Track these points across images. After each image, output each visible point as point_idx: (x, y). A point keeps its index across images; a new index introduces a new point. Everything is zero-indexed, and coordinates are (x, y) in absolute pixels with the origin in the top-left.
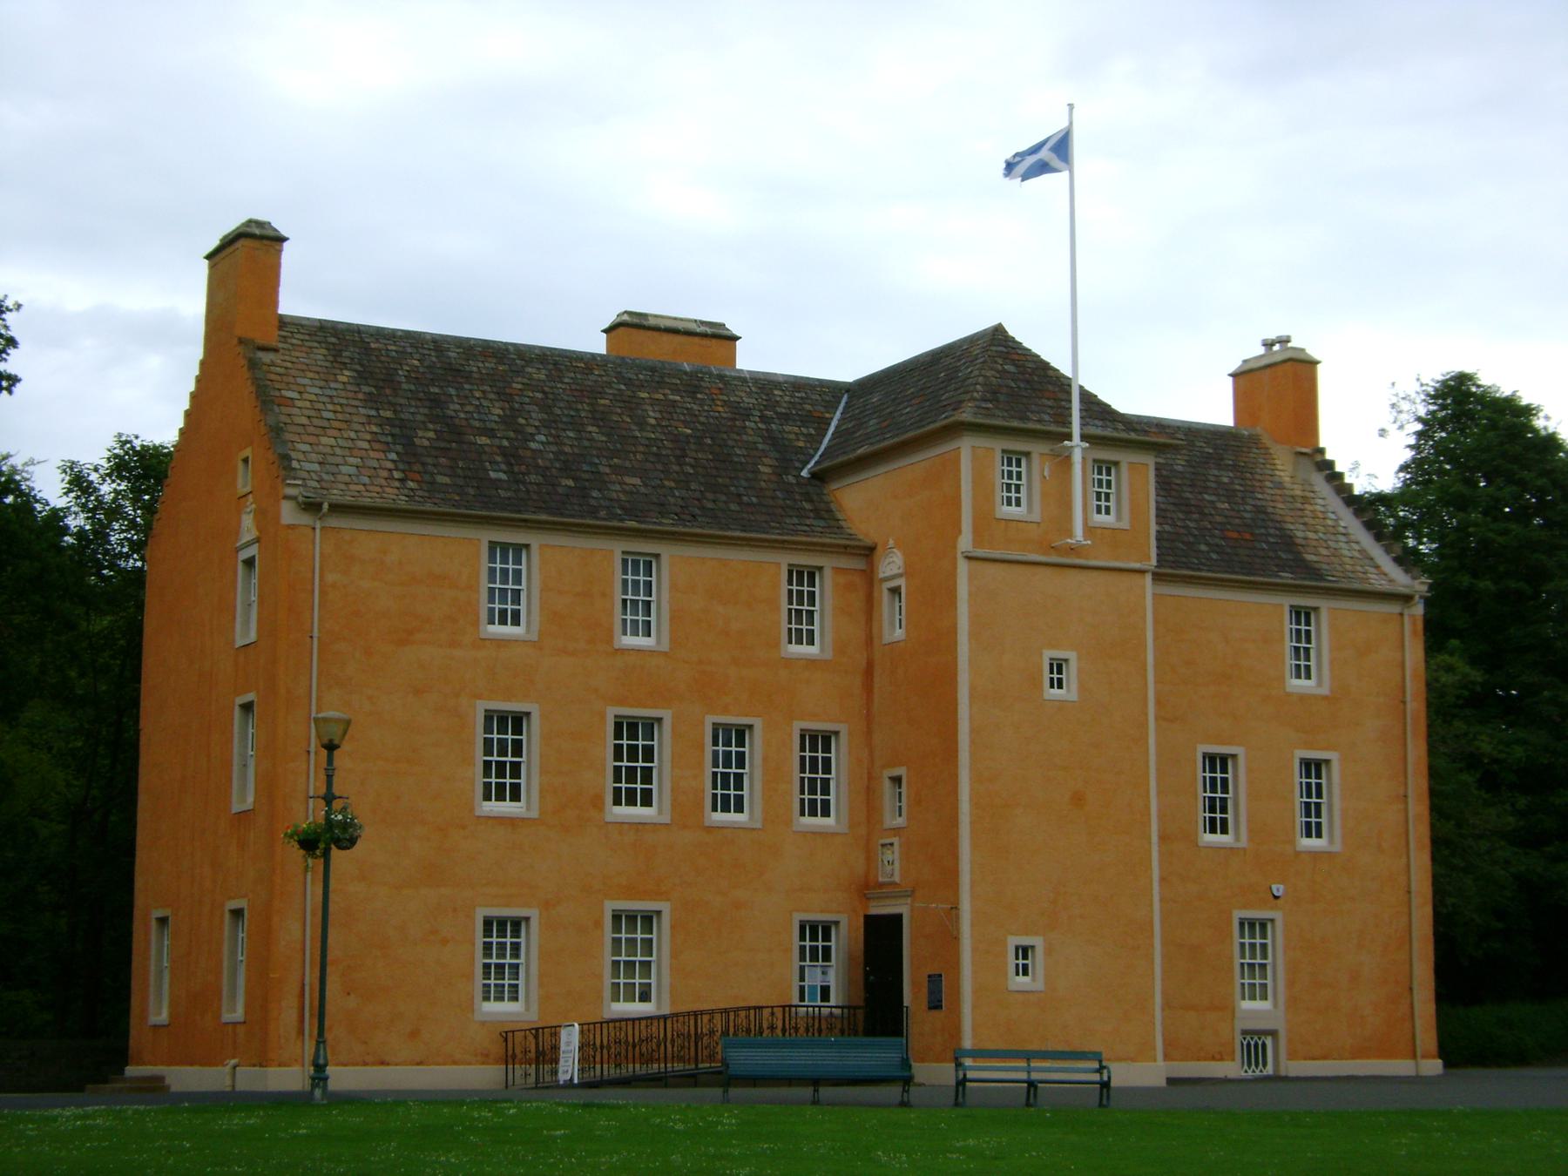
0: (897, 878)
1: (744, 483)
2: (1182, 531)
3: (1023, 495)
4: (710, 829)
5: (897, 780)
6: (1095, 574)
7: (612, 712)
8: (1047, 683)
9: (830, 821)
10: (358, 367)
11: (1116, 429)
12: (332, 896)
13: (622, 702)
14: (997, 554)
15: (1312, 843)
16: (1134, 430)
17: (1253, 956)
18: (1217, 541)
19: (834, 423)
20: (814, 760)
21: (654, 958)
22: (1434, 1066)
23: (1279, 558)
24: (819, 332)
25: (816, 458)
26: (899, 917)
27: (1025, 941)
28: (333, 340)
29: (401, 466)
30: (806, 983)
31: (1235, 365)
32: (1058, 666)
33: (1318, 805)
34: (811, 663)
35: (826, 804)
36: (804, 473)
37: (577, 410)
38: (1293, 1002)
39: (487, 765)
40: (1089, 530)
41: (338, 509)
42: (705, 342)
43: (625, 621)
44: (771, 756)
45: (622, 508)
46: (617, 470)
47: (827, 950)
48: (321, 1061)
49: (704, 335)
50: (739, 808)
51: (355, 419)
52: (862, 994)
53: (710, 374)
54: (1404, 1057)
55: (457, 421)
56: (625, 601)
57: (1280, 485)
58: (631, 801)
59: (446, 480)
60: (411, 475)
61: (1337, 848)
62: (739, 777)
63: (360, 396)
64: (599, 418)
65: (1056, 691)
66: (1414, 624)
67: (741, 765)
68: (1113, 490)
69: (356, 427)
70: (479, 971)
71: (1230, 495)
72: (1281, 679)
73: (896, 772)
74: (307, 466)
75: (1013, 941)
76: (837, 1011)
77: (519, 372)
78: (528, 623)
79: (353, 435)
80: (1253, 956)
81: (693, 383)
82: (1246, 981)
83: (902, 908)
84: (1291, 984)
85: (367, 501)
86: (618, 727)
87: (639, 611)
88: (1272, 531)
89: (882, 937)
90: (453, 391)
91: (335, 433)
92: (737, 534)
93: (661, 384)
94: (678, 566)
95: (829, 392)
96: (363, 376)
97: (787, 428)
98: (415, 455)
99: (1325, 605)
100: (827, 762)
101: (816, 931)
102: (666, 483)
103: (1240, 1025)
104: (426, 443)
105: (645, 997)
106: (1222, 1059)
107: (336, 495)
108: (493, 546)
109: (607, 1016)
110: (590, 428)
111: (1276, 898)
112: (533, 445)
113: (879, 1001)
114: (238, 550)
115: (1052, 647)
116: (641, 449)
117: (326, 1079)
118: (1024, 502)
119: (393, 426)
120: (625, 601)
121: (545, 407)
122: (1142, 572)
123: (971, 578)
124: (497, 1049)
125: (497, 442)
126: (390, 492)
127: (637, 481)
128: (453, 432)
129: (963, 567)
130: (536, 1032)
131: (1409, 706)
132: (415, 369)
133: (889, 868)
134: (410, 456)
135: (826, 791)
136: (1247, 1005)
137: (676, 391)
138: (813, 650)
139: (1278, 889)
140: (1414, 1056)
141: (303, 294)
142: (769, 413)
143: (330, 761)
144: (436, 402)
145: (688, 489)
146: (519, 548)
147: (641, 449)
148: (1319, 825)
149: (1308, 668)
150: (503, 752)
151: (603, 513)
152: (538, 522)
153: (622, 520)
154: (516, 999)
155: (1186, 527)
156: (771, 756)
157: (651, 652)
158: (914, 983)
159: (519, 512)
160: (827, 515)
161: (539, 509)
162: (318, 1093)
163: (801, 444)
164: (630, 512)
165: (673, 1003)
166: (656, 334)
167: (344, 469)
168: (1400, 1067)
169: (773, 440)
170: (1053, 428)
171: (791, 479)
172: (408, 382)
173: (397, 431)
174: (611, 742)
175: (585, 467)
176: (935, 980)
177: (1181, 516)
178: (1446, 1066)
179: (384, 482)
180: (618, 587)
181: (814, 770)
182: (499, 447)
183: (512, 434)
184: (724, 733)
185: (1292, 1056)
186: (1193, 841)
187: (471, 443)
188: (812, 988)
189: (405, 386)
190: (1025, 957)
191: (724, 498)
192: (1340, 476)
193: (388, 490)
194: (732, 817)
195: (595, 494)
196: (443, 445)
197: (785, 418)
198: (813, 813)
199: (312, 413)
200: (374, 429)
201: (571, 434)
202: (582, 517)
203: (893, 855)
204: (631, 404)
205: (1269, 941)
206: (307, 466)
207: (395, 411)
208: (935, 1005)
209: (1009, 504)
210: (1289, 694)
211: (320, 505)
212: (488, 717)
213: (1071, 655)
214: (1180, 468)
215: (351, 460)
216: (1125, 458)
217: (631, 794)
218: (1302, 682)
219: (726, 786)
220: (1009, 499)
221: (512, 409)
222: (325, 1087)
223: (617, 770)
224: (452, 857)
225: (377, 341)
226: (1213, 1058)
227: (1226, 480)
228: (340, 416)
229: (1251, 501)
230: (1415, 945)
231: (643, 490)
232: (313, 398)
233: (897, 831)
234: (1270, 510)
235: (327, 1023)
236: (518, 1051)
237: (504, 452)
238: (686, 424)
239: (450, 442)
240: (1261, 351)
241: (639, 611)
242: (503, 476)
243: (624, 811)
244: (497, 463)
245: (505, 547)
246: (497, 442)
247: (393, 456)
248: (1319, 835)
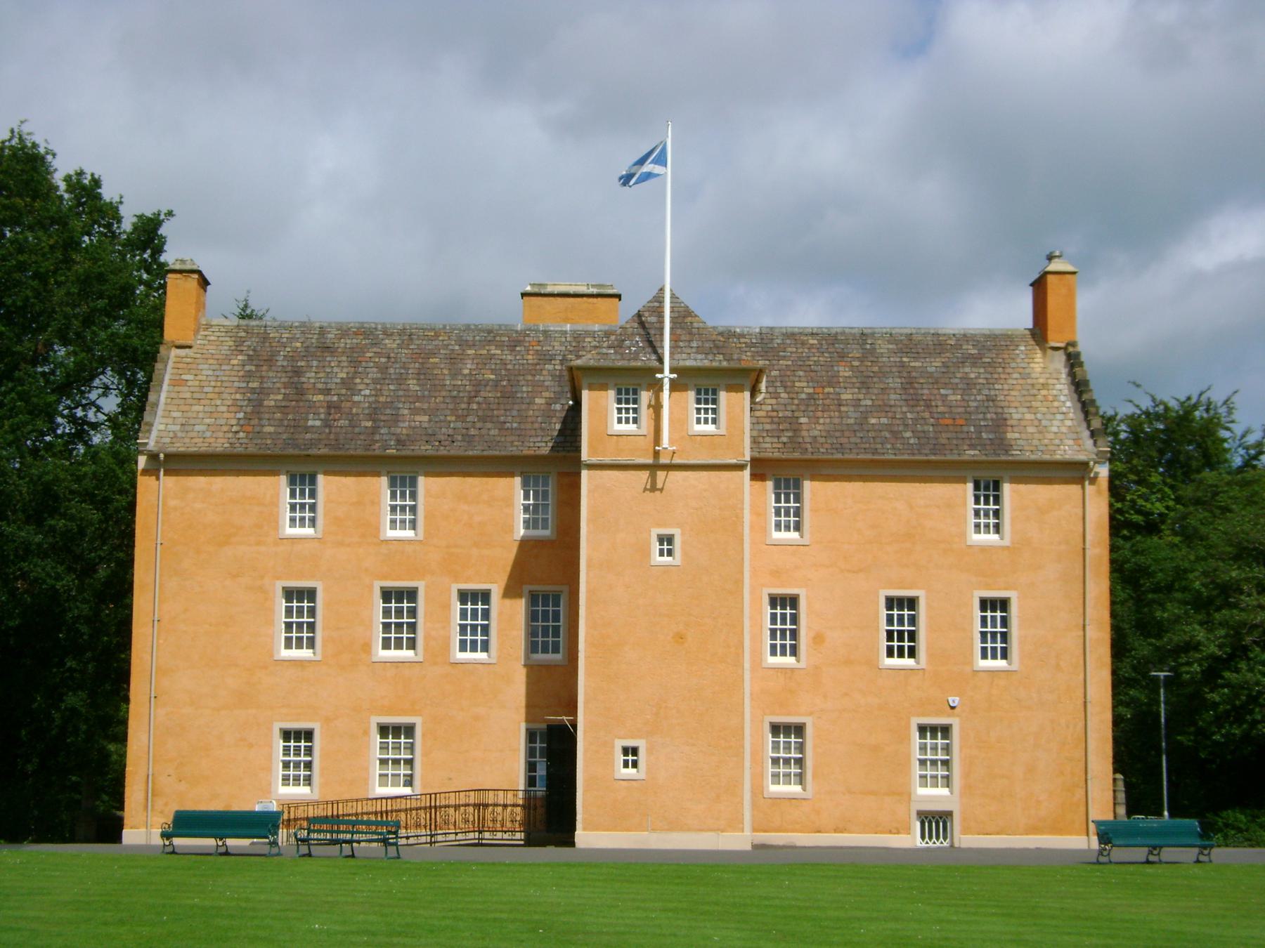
13: (385, 578)
27: (630, 743)
38: (968, 789)
53: (537, 331)
54: (1078, 834)
72: (963, 535)
84: (966, 775)
103: (915, 808)
111: (953, 708)
115: (659, 526)
122: (740, 467)
136: (922, 791)
137: (500, 346)
139: (954, 700)
150: (545, 619)
157: (410, 541)
165: (424, 786)
185: (966, 831)
186: (873, 664)
226: (890, 832)
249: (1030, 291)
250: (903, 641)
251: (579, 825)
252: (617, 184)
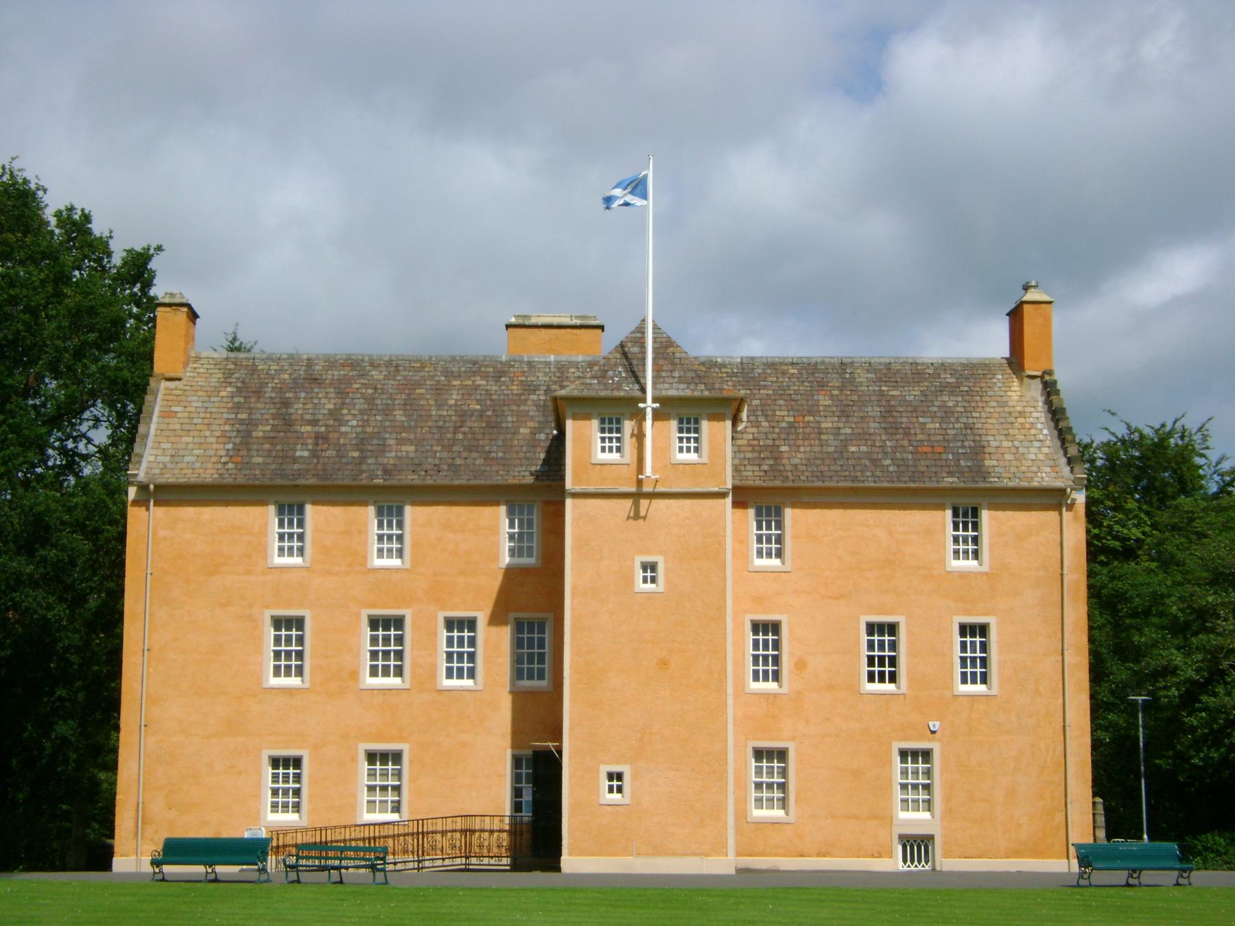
4: (442, 691)
13: (373, 606)
27: (615, 768)
38: (949, 813)
53: (521, 362)
61: (994, 692)
72: (943, 561)
84: (947, 799)
91: (197, 433)
103: (897, 831)
106: (881, 857)
111: (933, 732)
115: (642, 553)
122: (722, 495)
123: (574, 507)
136: (903, 815)
139: (935, 725)
157: (397, 570)
165: (411, 813)
166: (536, 330)
185: (947, 854)
186: (854, 689)
213: (659, 559)
226: (873, 856)
250: (884, 667)
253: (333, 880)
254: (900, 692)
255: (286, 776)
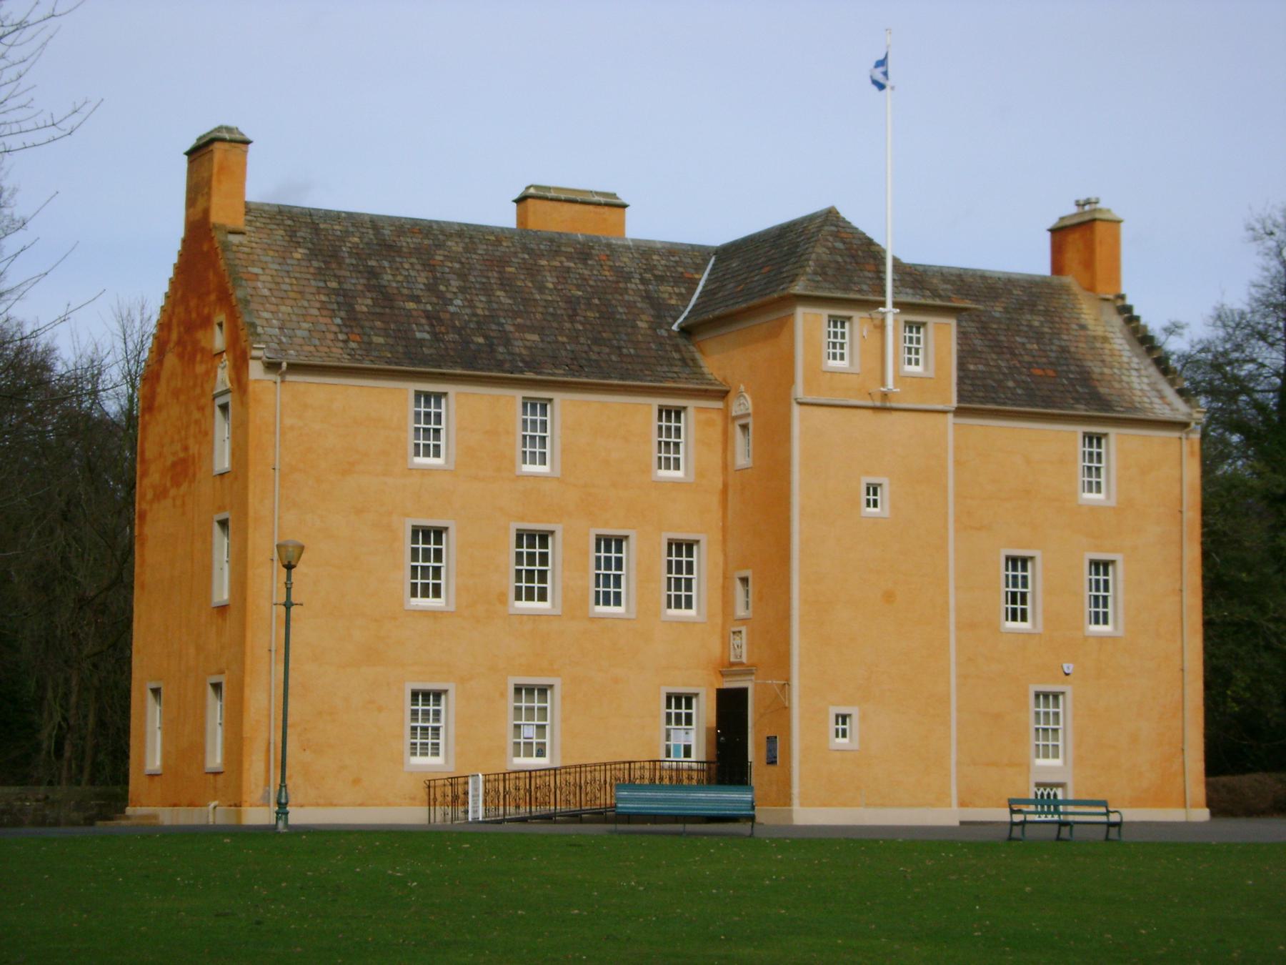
0: (744, 660)
1: (625, 338)
2: (994, 370)
3: (846, 351)
5: (745, 581)
6: (901, 414)
7: (514, 526)
8: (864, 503)
9: (692, 613)
10: (310, 245)
11: (924, 296)
12: (291, 673)
13: (522, 519)
14: (822, 400)
15: (1101, 628)
16: (940, 297)
17: (1047, 722)
18: (1024, 378)
19: (702, 283)
20: (679, 564)
21: (548, 722)
22: (1203, 814)
23: (1077, 392)
24: (690, 202)
25: (686, 313)
26: (743, 693)
28: (289, 222)
29: (345, 330)
30: (672, 743)
31: (1052, 221)
32: (873, 489)
33: (1105, 598)
34: (675, 484)
35: (689, 599)
36: (675, 327)
37: (488, 278)
39: (414, 569)
40: (899, 378)
41: (295, 368)
42: (600, 209)
43: (525, 453)
44: (644, 562)
45: (523, 361)
46: (520, 328)
47: (689, 717)
48: (283, 801)
49: (598, 204)
50: (618, 602)
51: (307, 290)
52: (714, 751)
55: (390, 291)
56: (524, 437)
57: (1083, 327)
58: (530, 597)
59: (381, 340)
60: (352, 337)
62: (618, 578)
63: (312, 270)
64: (506, 283)
65: (871, 509)
66: (1192, 446)
67: (619, 567)
68: (921, 345)
69: (309, 297)
70: (408, 731)
71: (1039, 337)
73: (744, 573)
74: (269, 330)
75: (834, 710)
76: (694, 765)
77: (439, 246)
78: (447, 454)
79: (306, 304)
80: (1047, 722)
81: (584, 252)
82: (1041, 743)
83: (748, 683)
85: (317, 362)
86: (519, 537)
87: (535, 445)
88: (1072, 368)
89: (732, 706)
90: (386, 264)
91: (292, 302)
92: (616, 382)
93: (557, 253)
94: (567, 408)
95: (699, 254)
96: (314, 253)
97: (662, 288)
98: (355, 319)
99: (1113, 432)
100: (690, 564)
101: (680, 700)
102: (560, 339)
104: (365, 309)
105: (541, 753)
107: (293, 356)
108: (418, 394)
109: (510, 768)
110: (498, 293)
111: (1067, 674)
112: (452, 309)
113: (728, 761)
114: (215, 397)
115: (867, 473)
116: (540, 310)
117: (287, 813)
118: (846, 356)
119: (338, 295)
120: (524, 437)
121: (462, 276)
122: (945, 412)
124: (422, 794)
125: (422, 307)
126: (337, 351)
127: (536, 337)
128: (385, 298)
129: (796, 410)
130: (452, 781)
131: (1185, 515)
132: (356, 246)
133: (738, 651)
134: (352, 320)
135: (689, 588)
136: (1041, 762)
137: (570, 258)
138: (680, 474)
139: (1068, 667)
140: (1185, 806)
141: (266, 180)
142: (648, 276)
143: (289, 577)
144: (373, 274)
145: (578, 343)
146: (439, 396)
147: (540, 310)
148: (1105, 614)
149: (1098, 484)
150: (426, 559)
151: (507, 365)
152: (455, 375)
153: (522, 372)
154: (437, 754)
155: (999, 367)
156: (644, 562)
158: (757, 745)
159: (440, 367)
160: (690, 364)
161: (455, 364)
162: (281, 824)
163: (673, 302)
164: (531, 365)
167: (299, 333)
168: (1174, 815)
169: (648, 297)
170: (871, 298)
171: (664, 333)
172: (350, 257)
173: (341, 299)
174: (513, 550)
175: (494, 327)
176: (771, 740)
177: (994, 356)
178: (1213, 814)
179: (330, 343)
180: (519, 425)
181: (679, 571)
182: (425, 311)
183: (435, 300)
184: (605, 542)
187: (399, 309)
188: (677, 747)
189: (348, 261)
190: (844, 723)
191: (606, 350)
192: (1137, 319)
193: (334, 350)
194: (612, 609)
195: (501, 349)
196: (378, 310)
197: (661, 279)
198: (678, 606)
199: (273, 286)
200: (323, 298)
201: (483, 299)
202: (490, 370)
203: (743, 640)
204: (532, 271)
205: (1060, 710)
206: (269, 330)
207: (339, 283)
208: (772, 761)
209: (834, 358)
210: (1080, 506)
211: (280, 364)
212: (415, 531)
213: (884, 481)
214: (997, 315)
215: (305, 325)
216: (931, 321)
217: (530, 592)
218: (1094, 496)
219: (607, 585)
220: (835, 355)
221: (435, 278)
222: (286, 819)
223: (519, 572)
224: (393, 638)
225: (325, 222)
227: (1036, 324)
228: (295, 288)
229: (1056, 342)
230: (1187, 714)
231: (541, 345)
232: (274, 273)
233: (744, 621)
234: (1073, 349)
235: (287, 774)
236: (438, 796)
237: (428, 316)
238: (578, 287)
239: (384, 307)
240: (1073, 210)
241: (535, 445)
242: (427, 336)
243: (524, 605)
244: (422, 325)
245: (428, 396)
246: (422, 307)
247: (338, 321)
248: (1106, 622)
249: (1046, 240)
250: (1017, 607)
251: (796, 801)
252: (883, 92)
253: (1068, 828)
254: (1036, 631)
255: (426, 713)
